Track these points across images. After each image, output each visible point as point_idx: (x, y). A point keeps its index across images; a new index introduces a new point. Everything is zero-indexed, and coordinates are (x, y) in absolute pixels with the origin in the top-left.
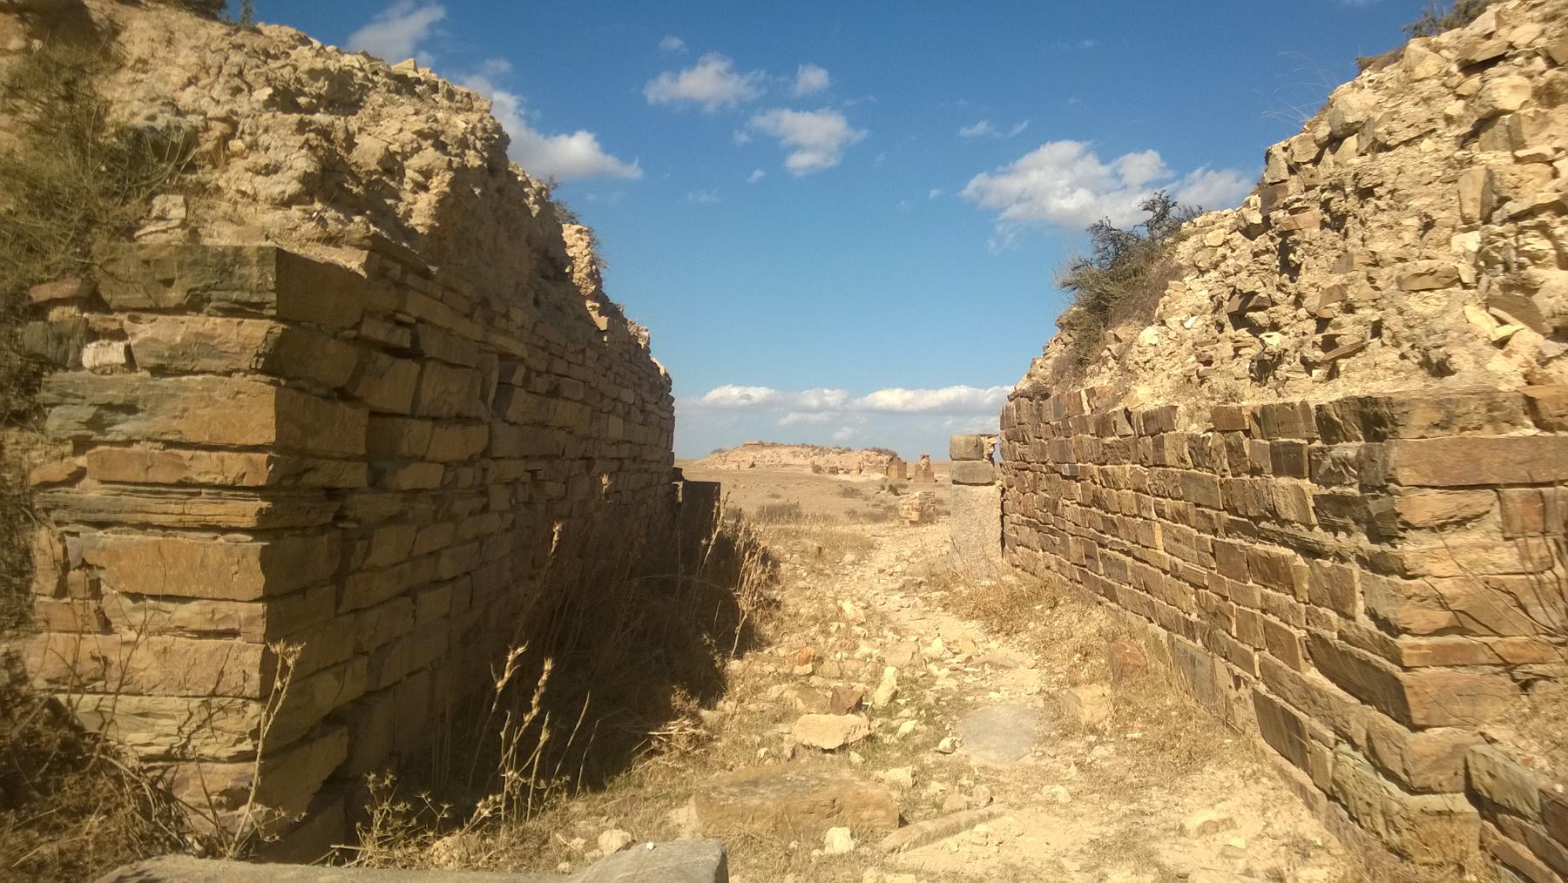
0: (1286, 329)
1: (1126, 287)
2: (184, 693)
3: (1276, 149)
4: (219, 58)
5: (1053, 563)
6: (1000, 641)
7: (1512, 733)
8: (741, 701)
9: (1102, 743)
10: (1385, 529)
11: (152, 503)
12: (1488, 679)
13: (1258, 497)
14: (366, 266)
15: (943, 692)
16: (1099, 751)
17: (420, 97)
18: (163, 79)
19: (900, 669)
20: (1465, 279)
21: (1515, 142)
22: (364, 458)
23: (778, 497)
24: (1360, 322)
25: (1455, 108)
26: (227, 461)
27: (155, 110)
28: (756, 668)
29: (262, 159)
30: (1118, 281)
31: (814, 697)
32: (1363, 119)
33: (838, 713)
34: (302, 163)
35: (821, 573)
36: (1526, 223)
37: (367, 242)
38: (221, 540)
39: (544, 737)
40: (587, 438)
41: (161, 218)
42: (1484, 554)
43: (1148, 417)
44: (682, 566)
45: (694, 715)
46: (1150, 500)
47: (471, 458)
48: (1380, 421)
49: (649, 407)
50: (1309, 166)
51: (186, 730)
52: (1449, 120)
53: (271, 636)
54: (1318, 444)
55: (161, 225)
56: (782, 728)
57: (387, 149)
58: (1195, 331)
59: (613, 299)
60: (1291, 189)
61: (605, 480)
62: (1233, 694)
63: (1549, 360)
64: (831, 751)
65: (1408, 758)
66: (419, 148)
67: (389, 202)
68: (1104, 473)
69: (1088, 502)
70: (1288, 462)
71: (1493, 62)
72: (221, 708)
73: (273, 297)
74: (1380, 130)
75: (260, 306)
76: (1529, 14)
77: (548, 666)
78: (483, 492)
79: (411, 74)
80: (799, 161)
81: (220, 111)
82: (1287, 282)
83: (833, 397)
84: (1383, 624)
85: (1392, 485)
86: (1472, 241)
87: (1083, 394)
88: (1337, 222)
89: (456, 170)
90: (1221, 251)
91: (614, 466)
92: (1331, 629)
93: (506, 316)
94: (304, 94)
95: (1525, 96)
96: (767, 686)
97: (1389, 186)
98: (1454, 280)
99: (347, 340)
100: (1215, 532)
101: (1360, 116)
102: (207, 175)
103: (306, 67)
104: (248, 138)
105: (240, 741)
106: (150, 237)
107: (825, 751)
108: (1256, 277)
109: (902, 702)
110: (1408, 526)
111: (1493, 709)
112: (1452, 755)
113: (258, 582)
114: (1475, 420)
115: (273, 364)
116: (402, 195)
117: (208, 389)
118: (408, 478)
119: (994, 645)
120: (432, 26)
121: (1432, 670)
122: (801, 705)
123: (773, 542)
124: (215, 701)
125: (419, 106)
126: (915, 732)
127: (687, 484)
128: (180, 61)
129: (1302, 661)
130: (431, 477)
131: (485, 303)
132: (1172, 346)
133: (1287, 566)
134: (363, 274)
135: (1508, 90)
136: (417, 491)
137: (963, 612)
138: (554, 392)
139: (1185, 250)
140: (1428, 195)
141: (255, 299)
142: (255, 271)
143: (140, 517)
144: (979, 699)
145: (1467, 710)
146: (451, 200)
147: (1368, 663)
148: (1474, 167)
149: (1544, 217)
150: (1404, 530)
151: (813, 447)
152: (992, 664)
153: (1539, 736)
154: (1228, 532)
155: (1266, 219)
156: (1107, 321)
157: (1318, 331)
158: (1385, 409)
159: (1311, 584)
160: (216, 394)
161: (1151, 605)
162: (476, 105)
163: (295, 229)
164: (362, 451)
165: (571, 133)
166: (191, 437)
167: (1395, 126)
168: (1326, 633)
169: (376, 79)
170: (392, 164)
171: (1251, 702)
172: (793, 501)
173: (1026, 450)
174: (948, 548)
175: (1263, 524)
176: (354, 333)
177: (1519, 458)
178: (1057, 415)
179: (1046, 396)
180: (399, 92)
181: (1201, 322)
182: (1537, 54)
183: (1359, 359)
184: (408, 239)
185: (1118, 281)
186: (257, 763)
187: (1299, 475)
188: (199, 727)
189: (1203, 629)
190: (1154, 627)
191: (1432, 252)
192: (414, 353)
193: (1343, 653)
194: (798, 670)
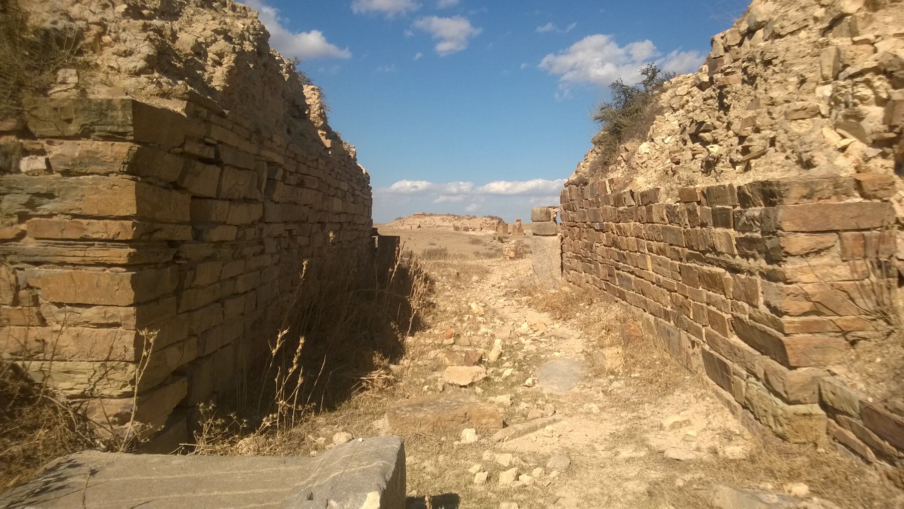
0: (721, 143)
1: (632, 120)
2: (91, 359)
3: (717, 37)
5: (590, 279)
8: (413, 359)
9: (617, 380)
10: (775, 256)
11: (66, 251)
14: (186, 110)
15: (528, 353)
16: (616, 384)
17: (216, 10)
19: (504, 341)
20: (823, 112)
21: (853, 32)
22: (190, 223)
23: (434, 244)
24: (763, 138)
25: (819, 12)
26: (109, 226)
27: (56, 18)
28: (422, 341)
29: (122, 47)
30: (627, 116)
31: (455, 357)
32: (767, 19)
33: (468, 365)
34: (146, 49)
35: (459, 287)
36: (858, 79)
37: (186, 96)
38: (108, 271)
39: (300, 381)
40: (320, 211)
42: (831, 270)
43: (643, 195)
44: (378, 284)
45: (386, 368)
46: (644, 242)
48: (772, 194)
49: (357, 192)
50: (736, 47)
51: (93, 380)
52: (816, 19)
53: (139, 326)
54: (738, 208)
55: (64, 87)
57: (196, 41)
60: (725, 61)
61: (331, 235)
62: (691, 351)
63: (870, 159)
64: (465, 387)
65: (787, 384)
66: (216, 40)
67: (199, 72)
68: (619, 228)
70: (722, 219)
72: (113, 368)
73: (131, 129)
74: (777, 26)
75: (124, 134)
77: (302, 341)
78: (261, 243)
80: (443, 47)
82: (723, 115)
84: (774, 310)
85: (779, 231)
86: (827, 91)
87: (607, 182)
88: (751, 80)
89: (237, 53)
90: (686, 98)
91: (337, 227)
92: (745, 313)
93: (271, 139)
94: (146, 8)
96: (428, 351)
97: (781, 59)
98: (816, 113)
99: (176, 154)
100: (681, 260)
102: (89, 57)
104: (113, 35)
105: (124, 386)
107: (461, 387)
108: (705, 113)
109: (505, 358)
110: (788, 254)
112: (812, 383)
113: (130, 295)
114: (827, 193)
115: (133, 168)
118: (215, 235)
119: (556, 326)
121: (801, 335)
122: (447, 361)
124: (109, 363)
125: (215, 14)
126: (512, 375)
127: (381, 237)
129: (729, 332)
130: (230, 234)
131: (258, 132)
132: (658, 154)
133: (721, 278)
134: (184, 115)
136: (223, 242)
138: (301, 184)
139: (665, 97)
140: (803, 64)
141: (121, 130)
142: (120, 113)
143: (60, 259)
144: (548, 356)
145: (820, 357)
146: (236, 71)
147: (765, 332)
148: (830, 47)
149: (868, 76)
150: (786, 257)
151: (454, 216)
152: (555, 337)
154: (688, 260)
155: (711, 79)
156: (620, 140)
157: (740, 143)
158: (776, 188)
159: (734, 288)
160: (100, 186)
161: (645, 302)
162: (249, 14)
163: (143, 89)
166: (87, 212)
167: (785, 23)
168: (742, 316)
170: (200, 50)
171: (700, 355)
172: (443, 247)
173: (575, 215)
174: (531, 272)
175: (708, 255)
176: (180, 150)
177: (851, 215)
178: (592, 194)
179: (586, 184)
180: (202, 7)
183: (762, 160)
184: (210, 95)
185: (627, 116)
186: (135, 398)
187: (727, 226)
188: (100, 379)
189: (674, 314)
190: (647, 315)
191: (805, 97)
192: (217, 162)
193: (752, 327)
194: (446, 342)
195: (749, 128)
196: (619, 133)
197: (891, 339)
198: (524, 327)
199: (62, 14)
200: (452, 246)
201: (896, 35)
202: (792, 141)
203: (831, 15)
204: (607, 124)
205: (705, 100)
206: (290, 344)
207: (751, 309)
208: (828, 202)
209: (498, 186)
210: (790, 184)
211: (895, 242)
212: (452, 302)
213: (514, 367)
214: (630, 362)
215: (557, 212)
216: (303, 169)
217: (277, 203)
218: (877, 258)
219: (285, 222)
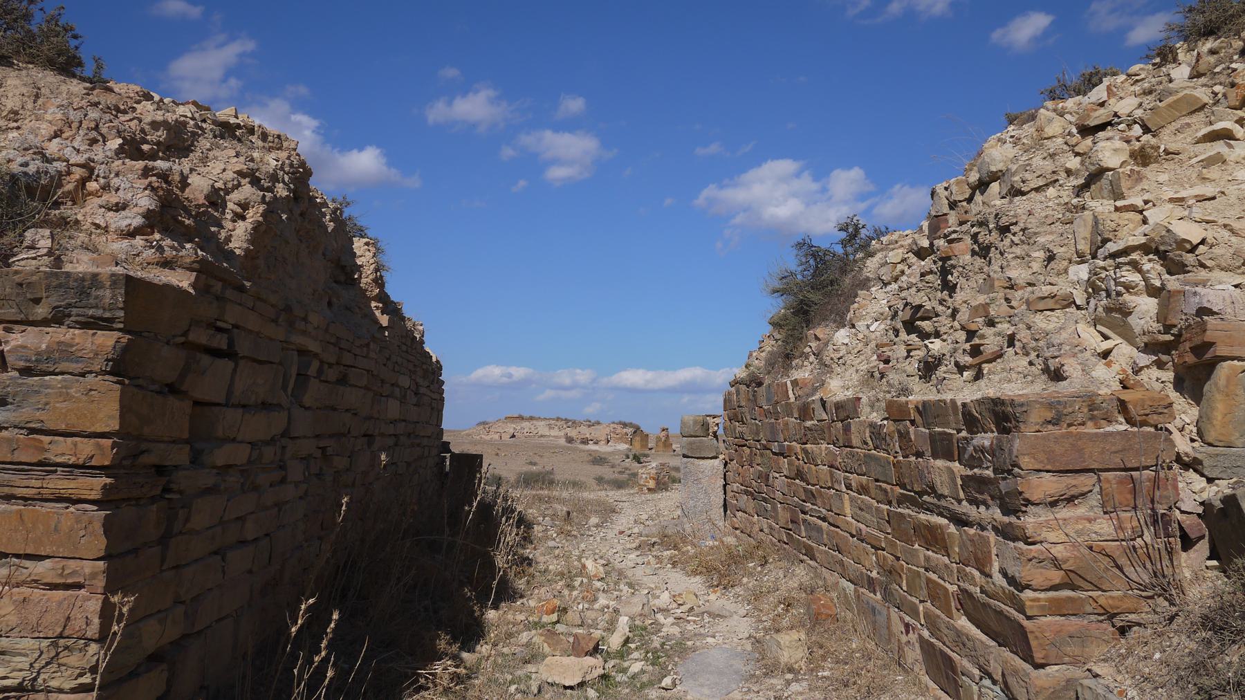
0: (945, 337)
1: (824, 295)
2: (37, 635)
3: (940, 188)
4: (80, 114)
5: (765, 526)
6: (718, 594)
7: (1112, 670)
8: (495, 645)
9: (797, 681)
10: (1013, 504)
11: (16, 479)
12: (1094, 625)
13: (921, 476)
14: (194, 285)
15: (668, 637)
16: (795, 687)
17: (239, 140)
18: (33, 131)
19: (632, 618)
20: (1078, 302)
21: (1117, 195)
22: (187, 442)
23: (535, 464)
24: (999, 334)
25: (1074, 163)
26: (80, 446)
27: (28, 158)
28: (510, 617)
29: (113, 198)
30: (818, 289)
31: (558, 642)
32: (1004, 169)
33: (578, 656)
34: (146, 202)
35: (569, 534)
36: (1121, 260)
37: (196, 266)
38: (72, 509)
39: (330, 674)
40: (369, 418)
41: (32, 247)
42: (1088, 525)
43: (839, 406)
44: (447, 529)
45: (455, 657)
46: (840, 475)
47: (272, 439)
48: (1006, 417)
49: (422, 390)
50: (965, 204)
51: (37, 666)
52: (1069, 172)
53: (110, 589)
54: (964, 434)
55: (32, 253)
56: (531, 668)
57: (213, 186)
58: (878, 334)
59: (393, 298)
60: (951, 222)
61: (383, 457)
62: (904, 639)
63: (1141, 369)
64: (571, 688)
65: (1032, 690)
66: (239, 185)
67: (213, 229)
68: (805, 451)
69: (793, 475)
70: (943, 448)
71: (1102, 127)
72: (66, 648)
73: (122, 314)
74: (1017, 178)
75: (111, 320)
76: (1132, 88)
77: (335, 616)
78: (282, 467)
79: (233, 120)
80: (557, 173)
81: (80, 159)
82: (947, 298)
83: (583, 376)
84: (1012, 581)
85: (1016, 469)
86: (1083, 272)
87: (789, 384)
88: (983, 251)
89: (267, 204)
90: (900, 267)
91: (391, 441)
92: (975, 585)
93: (305, 319)
94: (147, 142)
95: (1125, 156)
96: (519, 633)
97: (1021, 225)
98: (1069, 302)
99: (177, 345)
100: (890, 503)
101: (1001, 166)
102: (67, 211)
103: (149, 119)
104: (102, 181)
105: (81, 675)
106: (22, 263)
107: (566, 688)
108: (922, 293)
109: (633, 646)
110: (1028, 502)
111: (1097, 650)
112: (1066, 688)
113: (101, 544)
114: (1080, 417)
115: (119, 367)
116: (224, 223)
117: (66, 387)
118: (221, 456)
119: (713, 597)
120: (241, 55)
121: (1049, 618)
122: (547, 649)
123: (529, 506)
124: (62, 642)
125: (239, 147)
126: (643, 672)
127: (453, 455)
128: (48, 117)
129: (954, 611)
130: (240, 455)
131: (288, 309)
132: (860, 346)
133: (943, 533)
134: (192, 291)
135: (1110, 152)
136: (230, 466)
137: (689, 569)
138: (343, 380)
139: (872, 263)
140: (1051, 233)
141: (107, 315)
142: (108, 293)
143: (7, 490)
144: (698, 644)
145: (1077, 651)
146: (263, 228)
147: (1001, 613)
148: (1086, 213)
149: (1135, 256)
150: (1026, 506)
151: (567, 421)
152: (710, 614)
153: (1132, 673)
154: (899, 503)
155: (932, 244)
156: (808, 323)
157: (967, 341)
158: (1010, 409)
159: (960, 548)
160: (72, 391)
161: (842, 563)
162: (285, 144)
163: (138, 255)
164: (186, 435)
165: (361, 149)
166: (50, 425)
167: (1028, 176)
168: (971, 589)
169: (204, 125)
170: (216, 198)
171: (917, 645)
172: (548, 468)
173: (744, 429)
174: (679, 512)
175: (925, 498)
176: (182, 339)
177: (1113, 449)
178: (768, 400)
179: (760, 384)
180: (222, 137)
181: (883, 326)
182: (1135, 122)
183: (998, 365)
184: (227, 261)
185: (818, 289)
186: (95, 694)
187: (952, 459)
188: (47, 664)
189: (881, 583)
190: (844, 583)
191: (1054, 279)
192: (229, 354)
193: (985, 605)
194: (545, 619)
195: (980, 320)
196: (806, 313)
197: (1174, 626)
198: (665, 597)
199: (35, 153)
200: (563, 468)
201: (1171, 200)
202: (1037, 340)
203: (1087, 169)
204: (791, 299)
205: (923, 275)
206: (318, 618)
207: (983, 579)
208: (1081, 429)
209: (634, 377)
210: (1028, 404)
211: (1176, 488)
212: (557, 557)
213: (646, 659)
214: (817, 654)
215: (719, 423)
216: (348, 359)
217: (306, 409)
218: (1153, 509)
219: (317, 436)
